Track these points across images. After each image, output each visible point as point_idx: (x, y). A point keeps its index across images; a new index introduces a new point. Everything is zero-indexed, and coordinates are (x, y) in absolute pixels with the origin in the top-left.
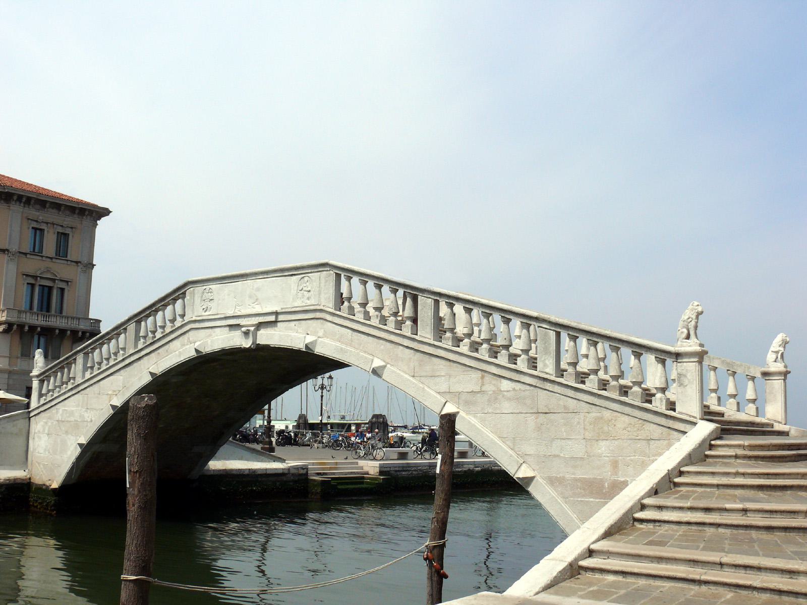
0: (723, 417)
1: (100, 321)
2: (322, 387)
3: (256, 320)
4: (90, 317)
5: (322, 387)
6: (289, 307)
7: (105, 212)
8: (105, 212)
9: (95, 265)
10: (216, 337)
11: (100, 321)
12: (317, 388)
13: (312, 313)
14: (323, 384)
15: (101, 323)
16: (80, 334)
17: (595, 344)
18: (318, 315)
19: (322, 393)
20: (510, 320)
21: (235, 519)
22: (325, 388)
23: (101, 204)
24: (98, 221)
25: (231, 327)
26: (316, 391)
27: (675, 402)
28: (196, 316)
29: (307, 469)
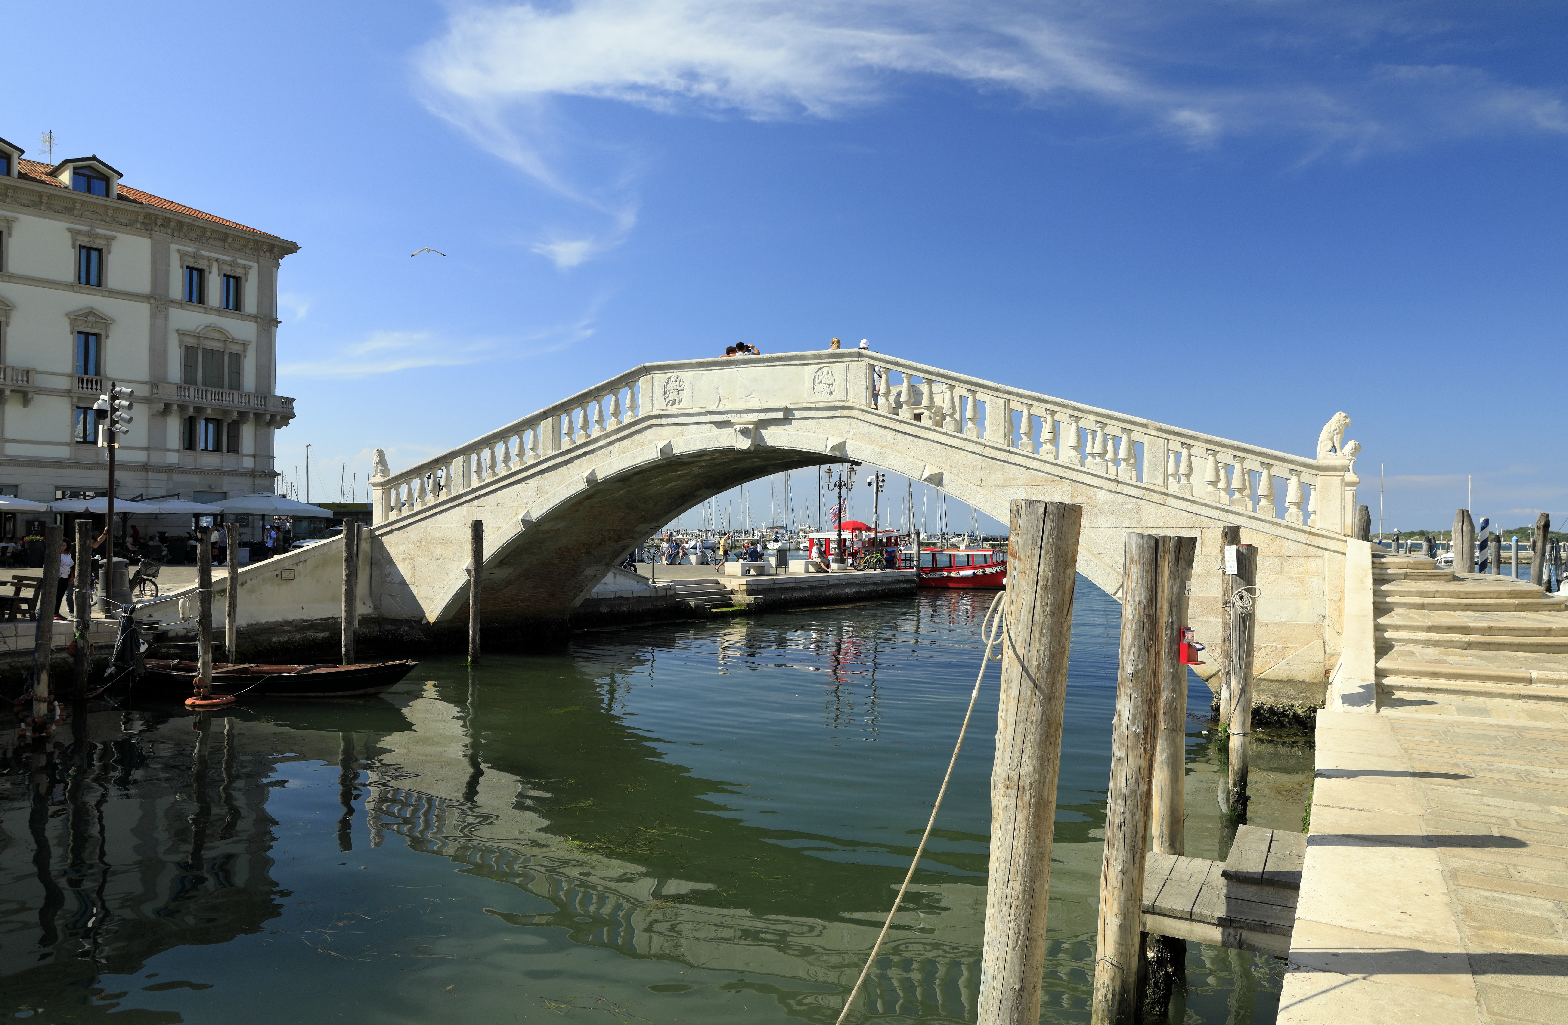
0: (278, 886)
1: (294, 400)
2: (840, 485)
3: (756, 417)
4: (277, 394)
5: (840, 485)
6: (805, 401)
7: (291, 248)
8: (291, 248)
9: (280, 322)
10: (691, 436)
11: (294, 400)
12: (832, 486)
13: (840, 410)
14: (840, 480)
15: (294, 403)
16: (268, 417)
17: (952, 387)
18: (846, 412)
19: (840, 492)
20: (954, 386)
21: (730, 622)
22: (845, 485)
23: (285, 235)
24: (280, 261)
25: (720, 424)
26: (830, 490)
27: (1080, 508)
28: (658, 410)
29: (675, 589)
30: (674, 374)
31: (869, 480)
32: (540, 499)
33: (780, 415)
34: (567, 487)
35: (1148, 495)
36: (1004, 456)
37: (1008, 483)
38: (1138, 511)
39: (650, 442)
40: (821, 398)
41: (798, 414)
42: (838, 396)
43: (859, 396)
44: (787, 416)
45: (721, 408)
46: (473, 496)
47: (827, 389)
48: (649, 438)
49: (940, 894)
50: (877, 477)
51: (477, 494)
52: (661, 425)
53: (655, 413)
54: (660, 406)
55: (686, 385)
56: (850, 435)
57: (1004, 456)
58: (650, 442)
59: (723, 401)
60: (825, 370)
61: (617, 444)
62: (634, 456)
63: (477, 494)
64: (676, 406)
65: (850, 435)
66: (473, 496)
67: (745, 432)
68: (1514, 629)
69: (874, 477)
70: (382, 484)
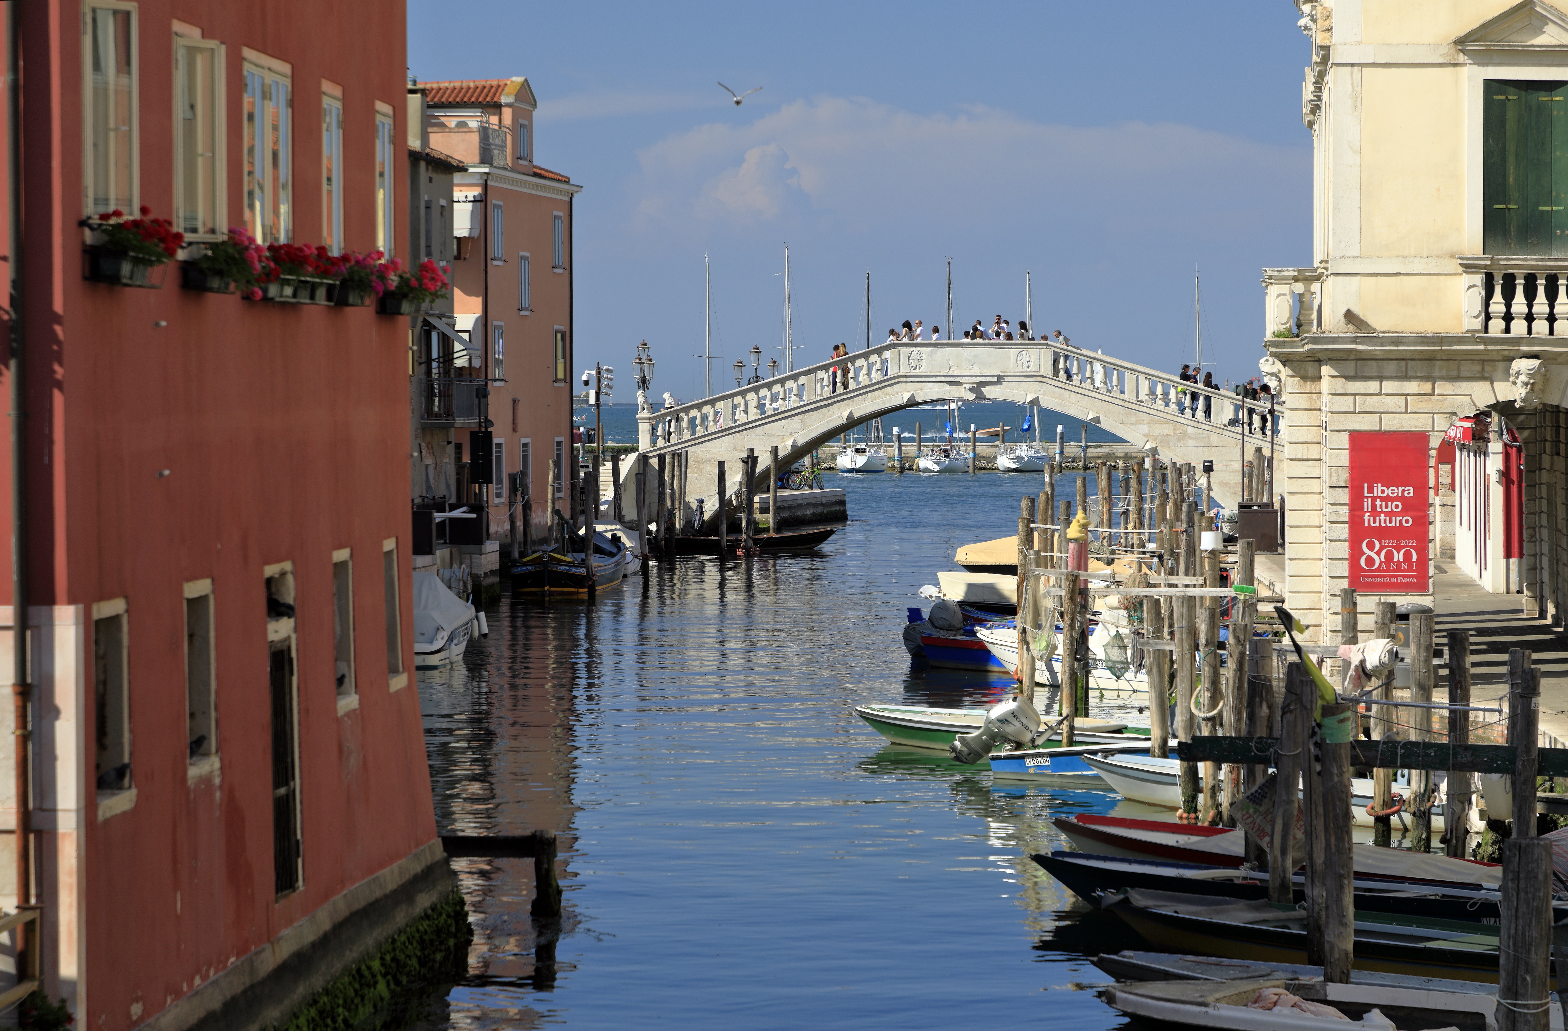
3: (978, 380)
25: (950, 383)
30: (916, 349)
31: (585, 377)
32: (804, 431)
33: (995, 379)
34: (828, 422)
35: (1214, 429)
36: (1136, 407)
37: (1138, 423)
38: (1209, 437)
39: (897, 393)
40: (1022, 369)
41: (1007, 379)
42: (1033, 368)
43: (1047, 368)
44: (1000, 380)
45: (951, 373)
46: (743, 428)
47: (1025, 364)
48: (896, 390)
49: (1177, 575)
50: (599, 373)
51: (746, 427)
52: (906, 382)
53: (901, 374)
54: (904, 369)
55: (924, 356)
56: (1041, 393)
57: (1136, 407)
58: (897, 393)
59: (953, 369)
60: (1024, 353)
61: (870, 394)
62: (884, 402)
63: (746, 427)
64: (918, 370)
65: (1041, 393)
66: (743, 428)
67: (971, 390)
68: (1362, 931)
69: (594, 373)
70: (649, 419)
